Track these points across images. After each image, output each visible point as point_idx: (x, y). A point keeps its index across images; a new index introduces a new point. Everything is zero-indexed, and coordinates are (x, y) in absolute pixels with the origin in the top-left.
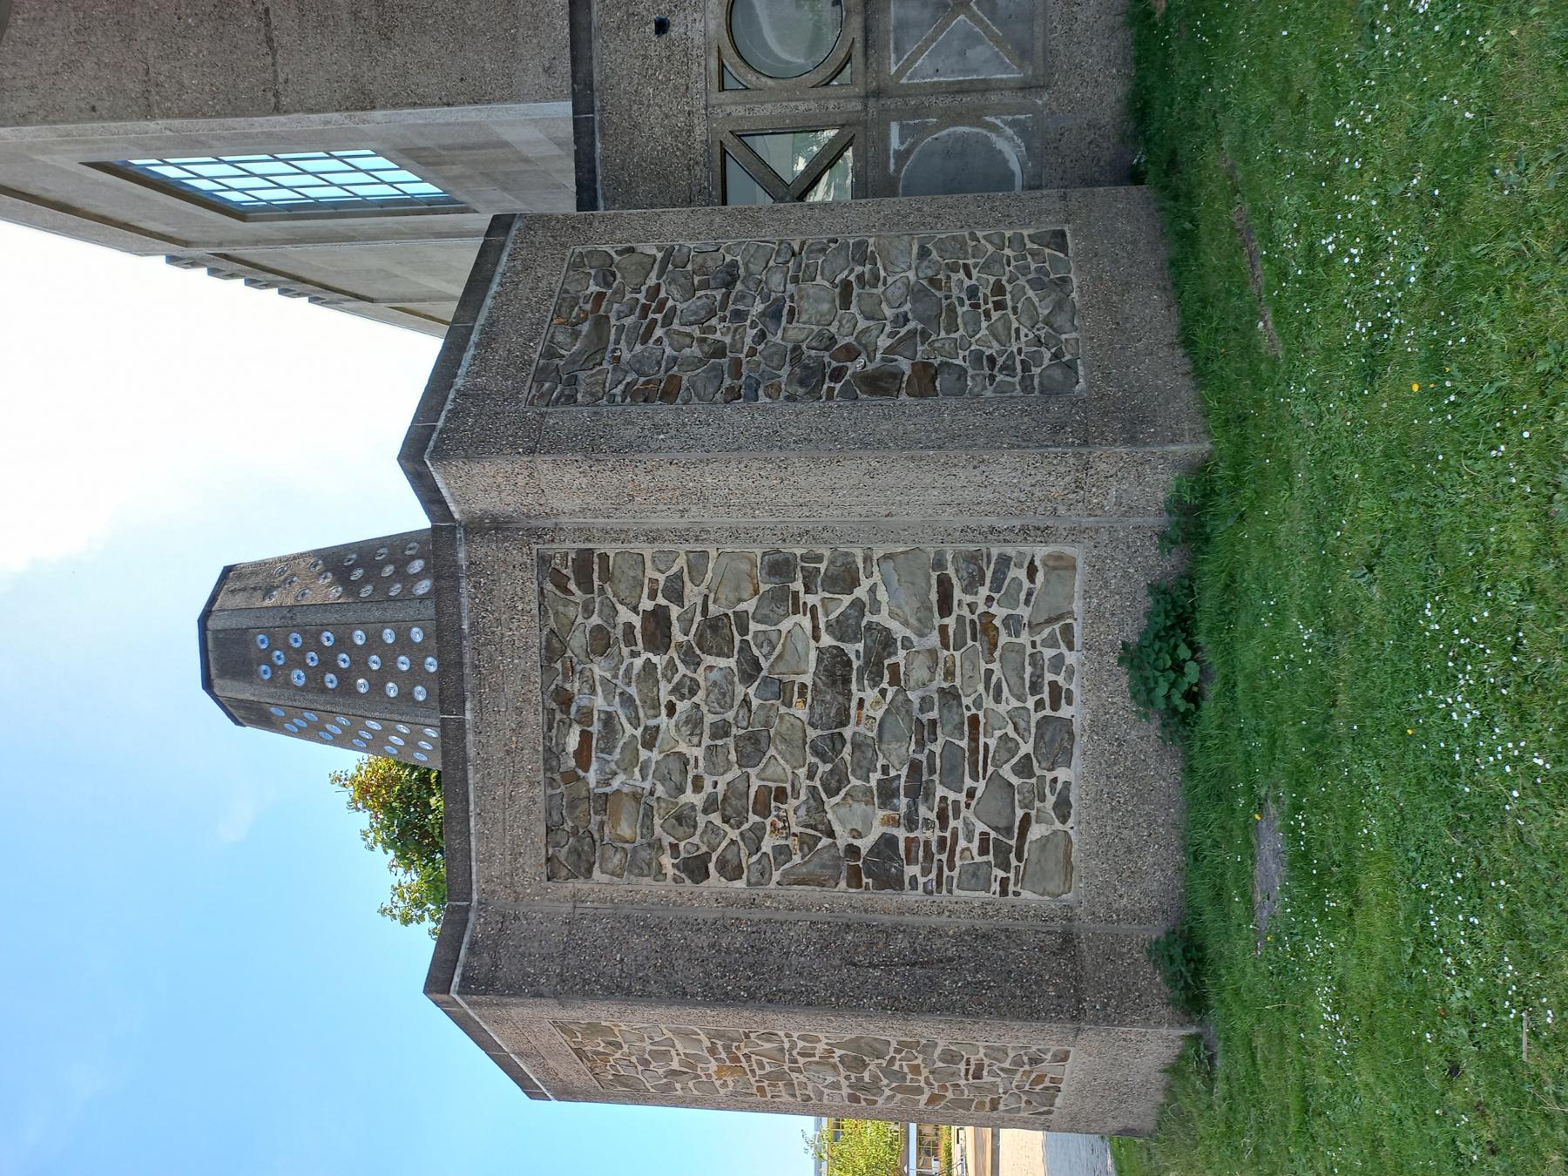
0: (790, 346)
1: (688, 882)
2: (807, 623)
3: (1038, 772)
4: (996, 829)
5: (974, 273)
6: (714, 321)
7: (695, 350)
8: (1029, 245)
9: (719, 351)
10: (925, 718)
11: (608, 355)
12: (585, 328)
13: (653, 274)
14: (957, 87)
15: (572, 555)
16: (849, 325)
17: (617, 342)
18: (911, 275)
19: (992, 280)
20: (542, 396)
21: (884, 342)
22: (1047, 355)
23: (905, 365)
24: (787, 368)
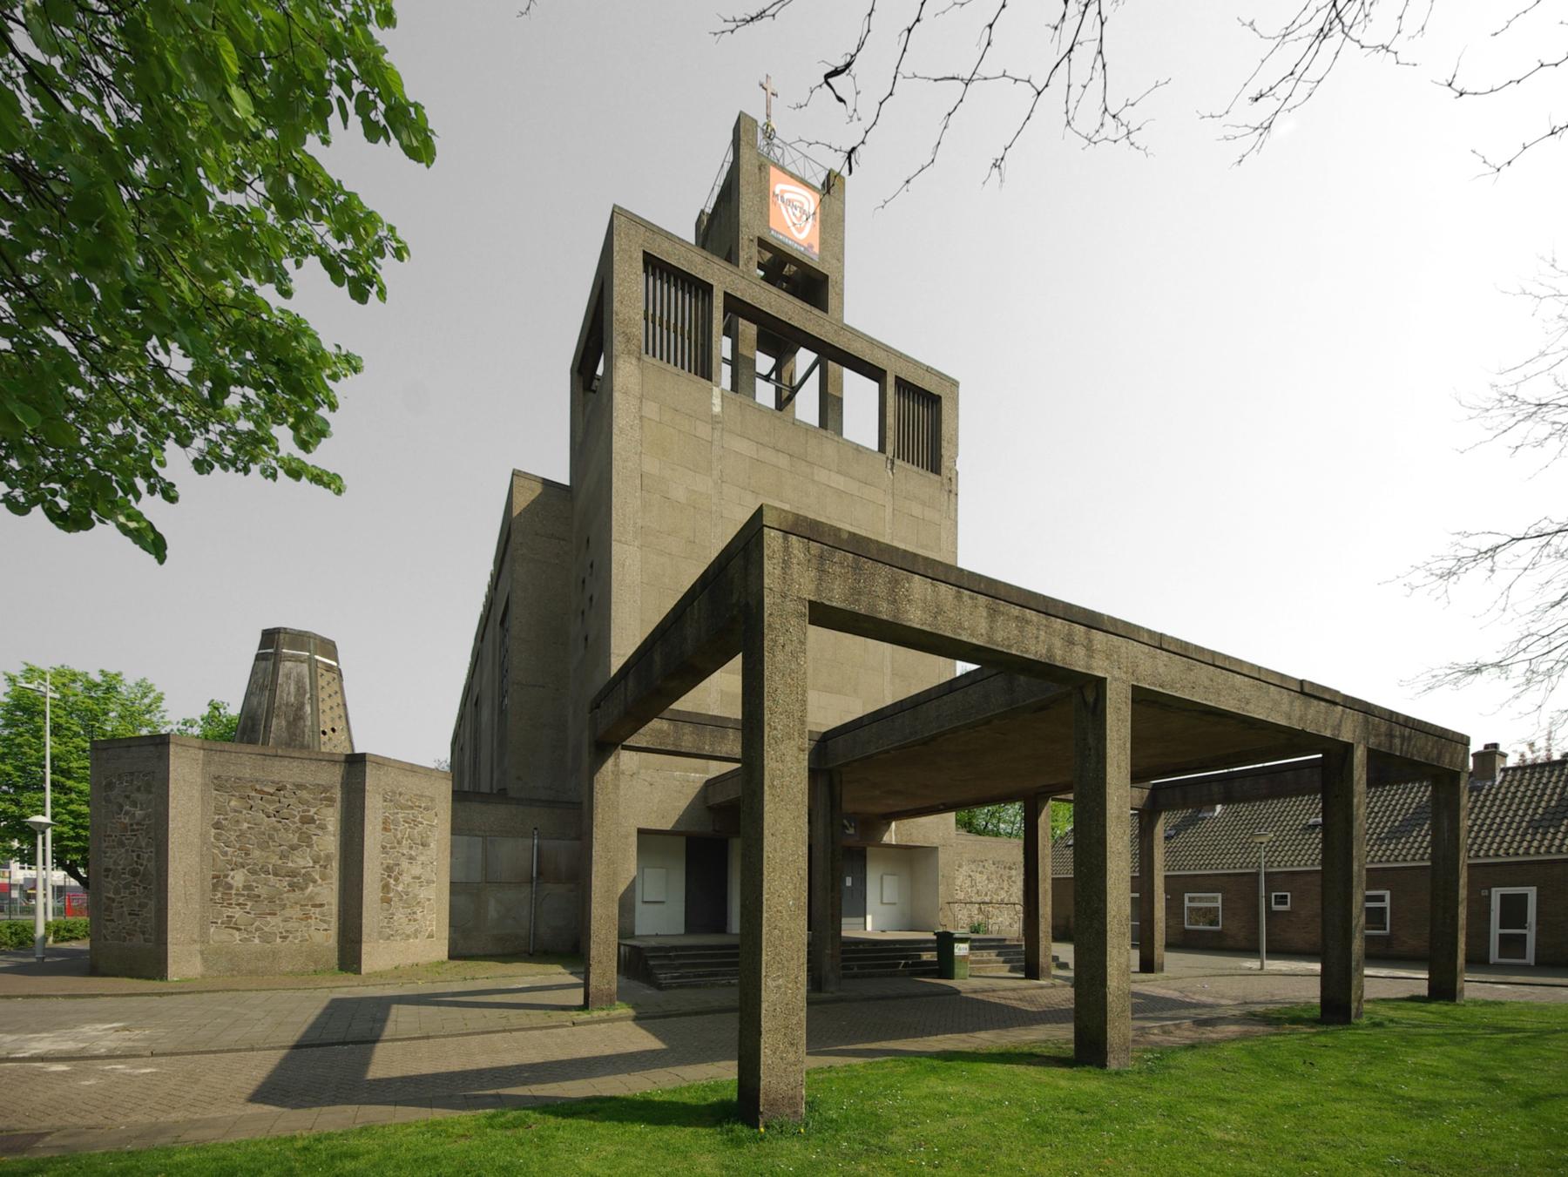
16: (406, 878)
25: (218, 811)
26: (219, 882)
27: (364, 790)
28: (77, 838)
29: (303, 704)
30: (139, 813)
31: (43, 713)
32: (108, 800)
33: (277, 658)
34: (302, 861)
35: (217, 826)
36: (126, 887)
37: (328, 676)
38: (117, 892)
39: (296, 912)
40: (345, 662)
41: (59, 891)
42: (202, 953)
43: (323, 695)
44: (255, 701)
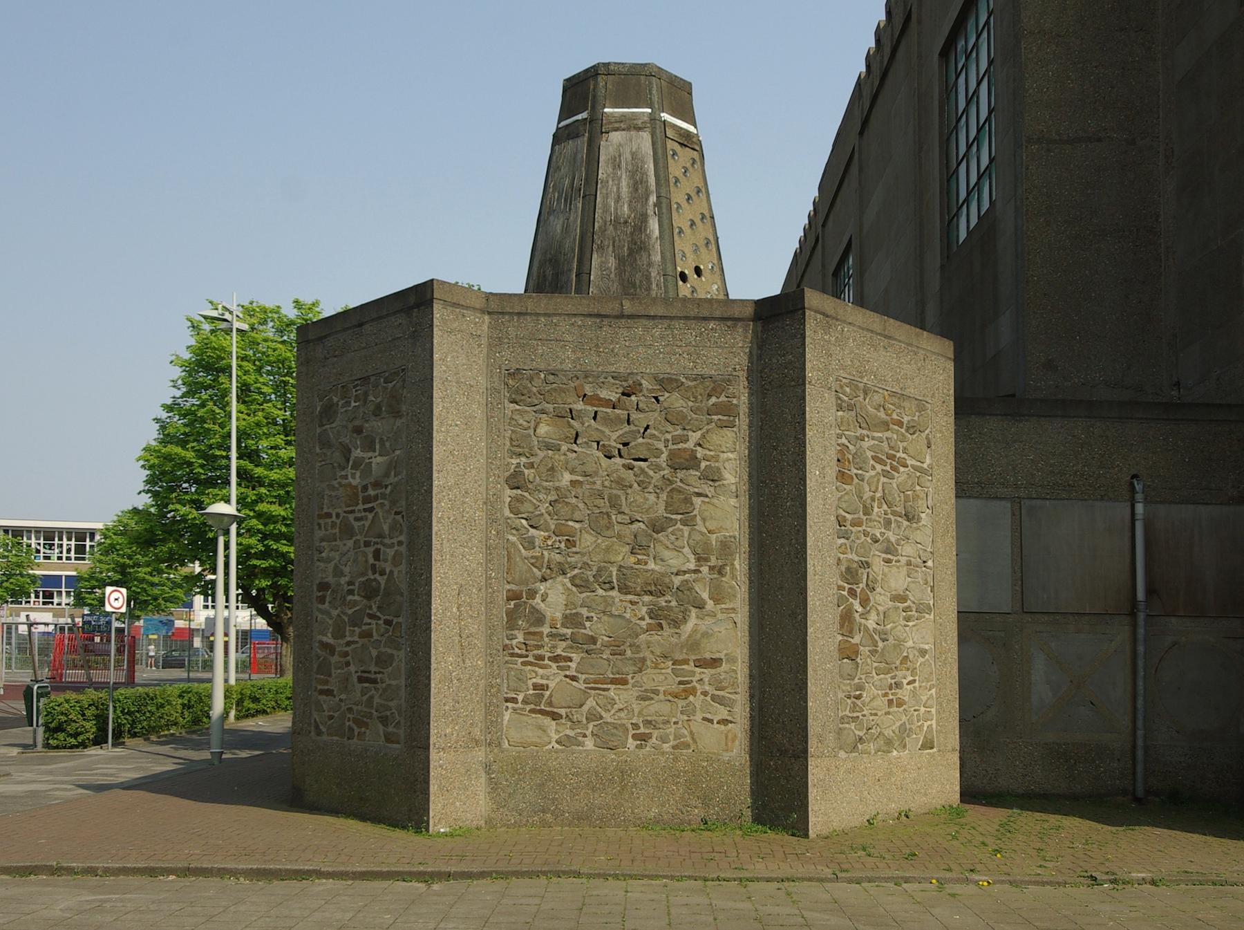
0: (869, 560)
1: (507, 474)
2: (692, 566)
3: (591, 726)
4: (551, 696)
5: (911, 687)
6: (885, 507)
7: (867, 495)
8: (926, 724)
9: (867, 511)
10: (626, 647)
11: (865, 432)
12: (882, 415)
13: (914, 462)
14: (586, 269)
15: (735, 401)
16: (881, 599)
17: (873, 438)
18: (910, 644)
19: (906, 699)
20: (841, 387)
21: (871, 624)
22: (861, 734)
23: (856, 639)
24: (856, 559)
25: (519, 446)
26: (520, 608)
27: (801, 381)
28: (266, 554)
29: (644, 218)
30: (378, 461)
31: (227, 370)
32: (325, 443)
33: (595, 129)
34: (672, 558)
35: (516, 481)
36: (355, 621)
37: (685, 155)
38: (339, 633)
39: (662, 678)
40: (708, 124)
41: (245, 637)
42: (488, 768)
43: (678, 196)
44: (557, 225)
